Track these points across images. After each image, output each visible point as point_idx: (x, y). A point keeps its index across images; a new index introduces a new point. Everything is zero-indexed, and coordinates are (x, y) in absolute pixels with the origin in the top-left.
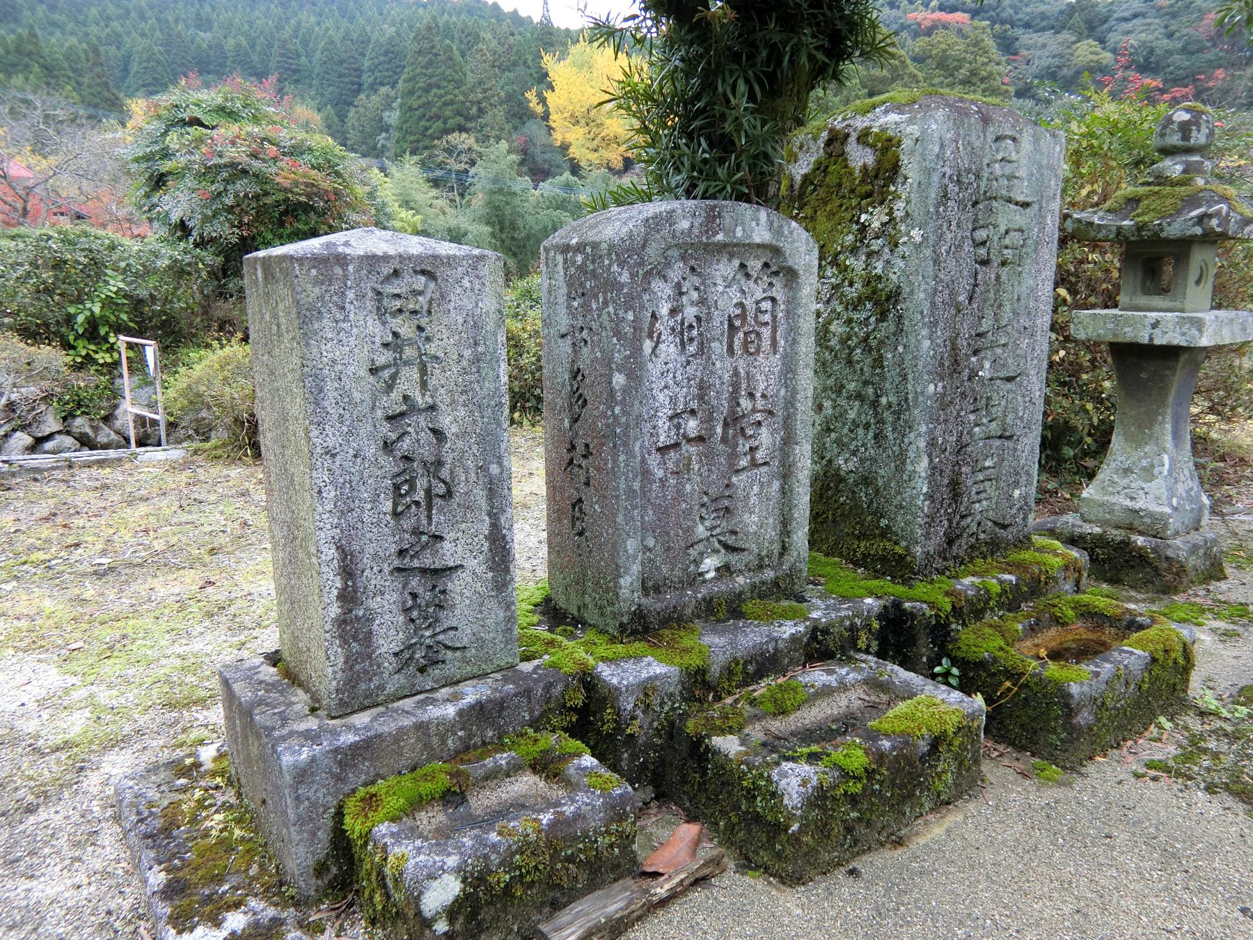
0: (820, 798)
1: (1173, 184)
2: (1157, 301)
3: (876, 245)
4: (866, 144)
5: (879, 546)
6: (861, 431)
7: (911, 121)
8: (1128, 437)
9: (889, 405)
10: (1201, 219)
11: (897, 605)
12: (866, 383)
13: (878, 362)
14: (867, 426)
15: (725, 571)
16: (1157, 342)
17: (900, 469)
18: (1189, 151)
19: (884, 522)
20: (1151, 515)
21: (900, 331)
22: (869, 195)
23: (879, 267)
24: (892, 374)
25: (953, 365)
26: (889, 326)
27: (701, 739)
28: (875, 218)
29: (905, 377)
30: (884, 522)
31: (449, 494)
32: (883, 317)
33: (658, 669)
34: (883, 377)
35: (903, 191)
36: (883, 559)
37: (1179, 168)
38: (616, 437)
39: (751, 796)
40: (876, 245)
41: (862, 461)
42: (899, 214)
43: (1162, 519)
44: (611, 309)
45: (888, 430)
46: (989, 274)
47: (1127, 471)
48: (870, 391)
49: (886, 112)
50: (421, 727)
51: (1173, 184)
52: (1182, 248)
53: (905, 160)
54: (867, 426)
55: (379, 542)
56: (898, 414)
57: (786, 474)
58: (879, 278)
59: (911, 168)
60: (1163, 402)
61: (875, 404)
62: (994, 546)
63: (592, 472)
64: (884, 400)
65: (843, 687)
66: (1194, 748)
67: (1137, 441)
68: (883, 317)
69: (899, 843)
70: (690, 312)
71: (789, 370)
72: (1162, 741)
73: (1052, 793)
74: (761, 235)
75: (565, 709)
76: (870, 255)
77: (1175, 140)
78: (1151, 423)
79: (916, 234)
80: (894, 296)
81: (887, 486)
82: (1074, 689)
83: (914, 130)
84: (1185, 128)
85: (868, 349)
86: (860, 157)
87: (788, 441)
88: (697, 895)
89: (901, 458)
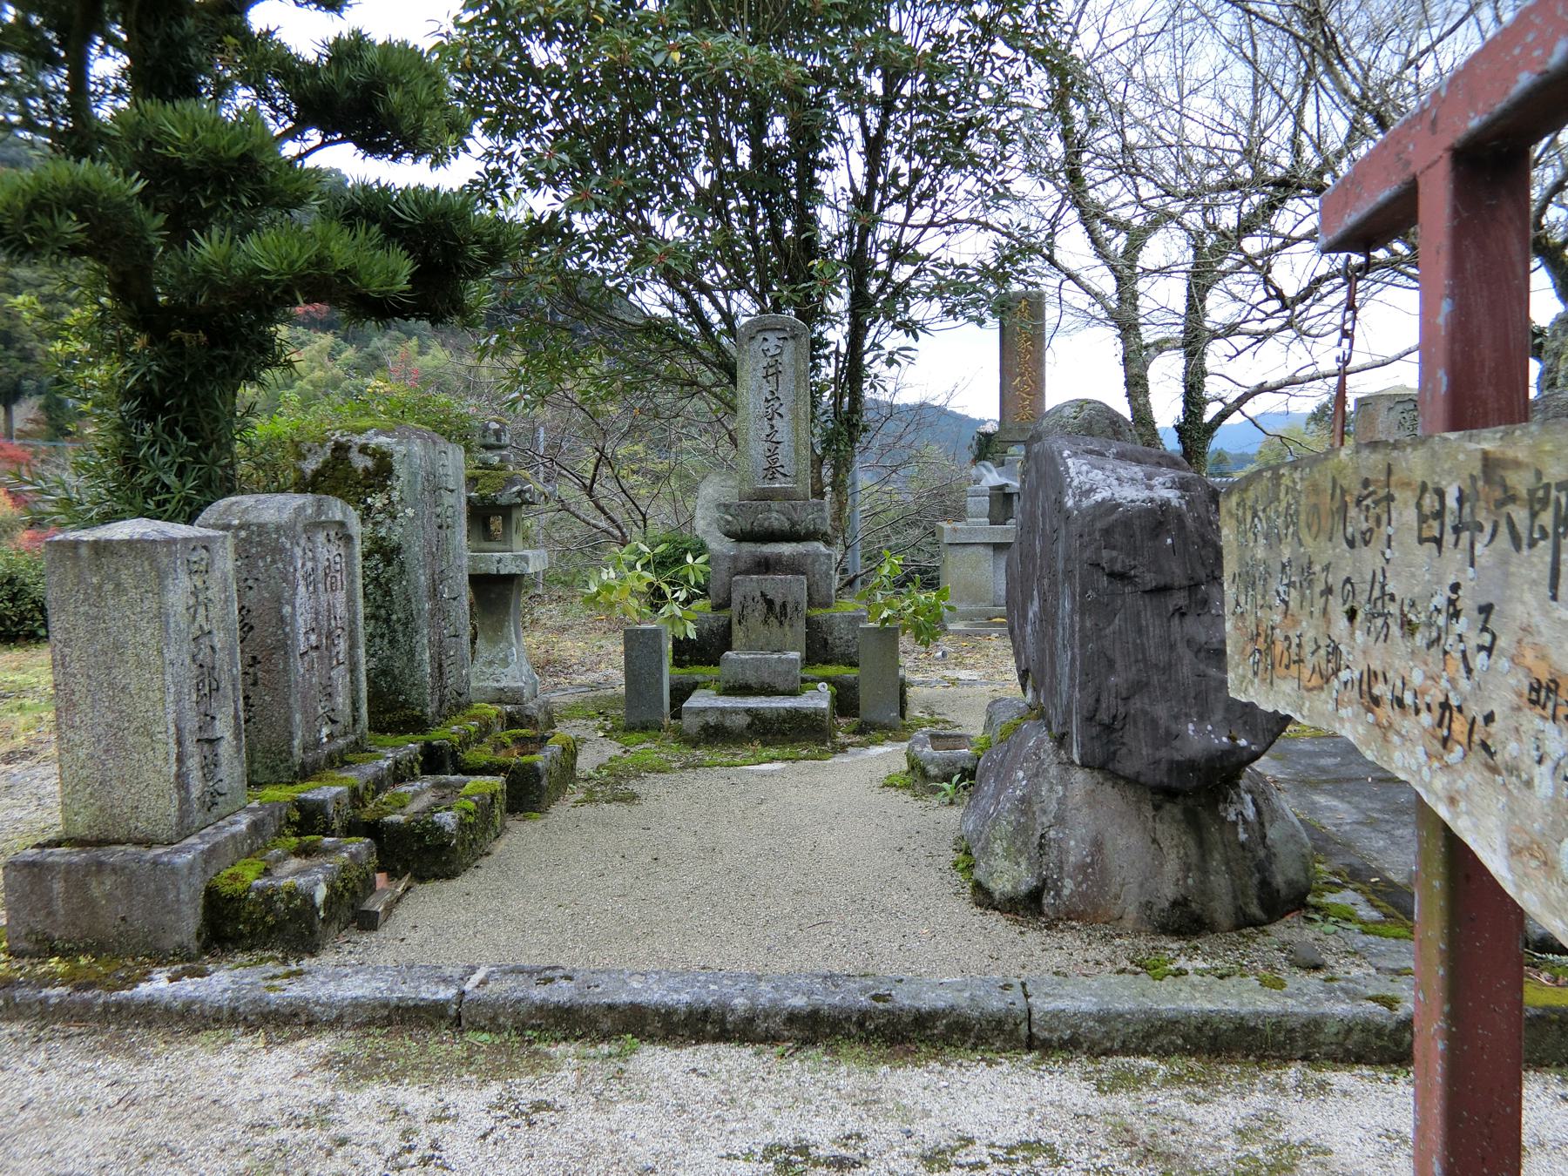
0: (462, 825)
1: (495, 469)
2: (493, 545)
3: (379, 518)
4: (366, 454)
5: (400, 715)
6: (377, 640)
7: (399, 443)
8: (489, 640)
9: (399, 620)
10: (520, 493)
11: (428, 745)
12: (379, 607)
13: (388, 593)
14: (382, 636)
15: (331, 736)
16: (502, 572)
17: (411, 659)
18: (501, 447)
19: (402, 698)
20: (512, 689)
21: (402, 571)
22: (371, 486)
23: (383, 532)
24: (399, 600)
25: (434, 593)
26: (393, 569)
27: (377, 822)
28: (378, 501)
29: (409, 601)
30: (402, 698)
31: (217, 689)
32: (389, 563)
33: (339, 789)
34: (392, 602)
35: (398, 485)
36: (404, 723)
37: (497, 459)
38: (283, 646)
39: (421, 837)
40: (379, 518)
41: (380, 660)
42: (395, 499)
43: (519, 691)
44: (280, 565)
45: (400, 637)
46: (443, 533)
47: (491, 663)
48: (383, 612)
49: (376, 435)
50: (233, 836)
51: (495, 469)
52: (506, 511)
53: (396, 466)
54: (382, 636)
55: (192, 722)
56: (406, 625)
57: (353, 669)
58: (383, 539)
59: (400, 469)
60: (507, 613)
61: (387, 620)
62: (459, 707)
63: (260, 674)
64: (394, 617)
65: (423, 792)
66: (590, 792)
67: (494, 642)
68: (389, 563)
69: (488, 854)
70: (309, 565)
71: (351, 600)
72: (576, 793)
73: (541, 823)
74: (339, 517)
75: (289, 823)
76: (375, 524)
77: (492, 440)
78: (502, 627)
79: (410, 512)
80: (397, 549)
81: (401, 673)
82: (540, 764)
83: (402, 449)
84: (497, 433)
85: (379, 585)
86: (361, 462)
87: (353, 647)
88: (801, 529)
89: (411, 653)
